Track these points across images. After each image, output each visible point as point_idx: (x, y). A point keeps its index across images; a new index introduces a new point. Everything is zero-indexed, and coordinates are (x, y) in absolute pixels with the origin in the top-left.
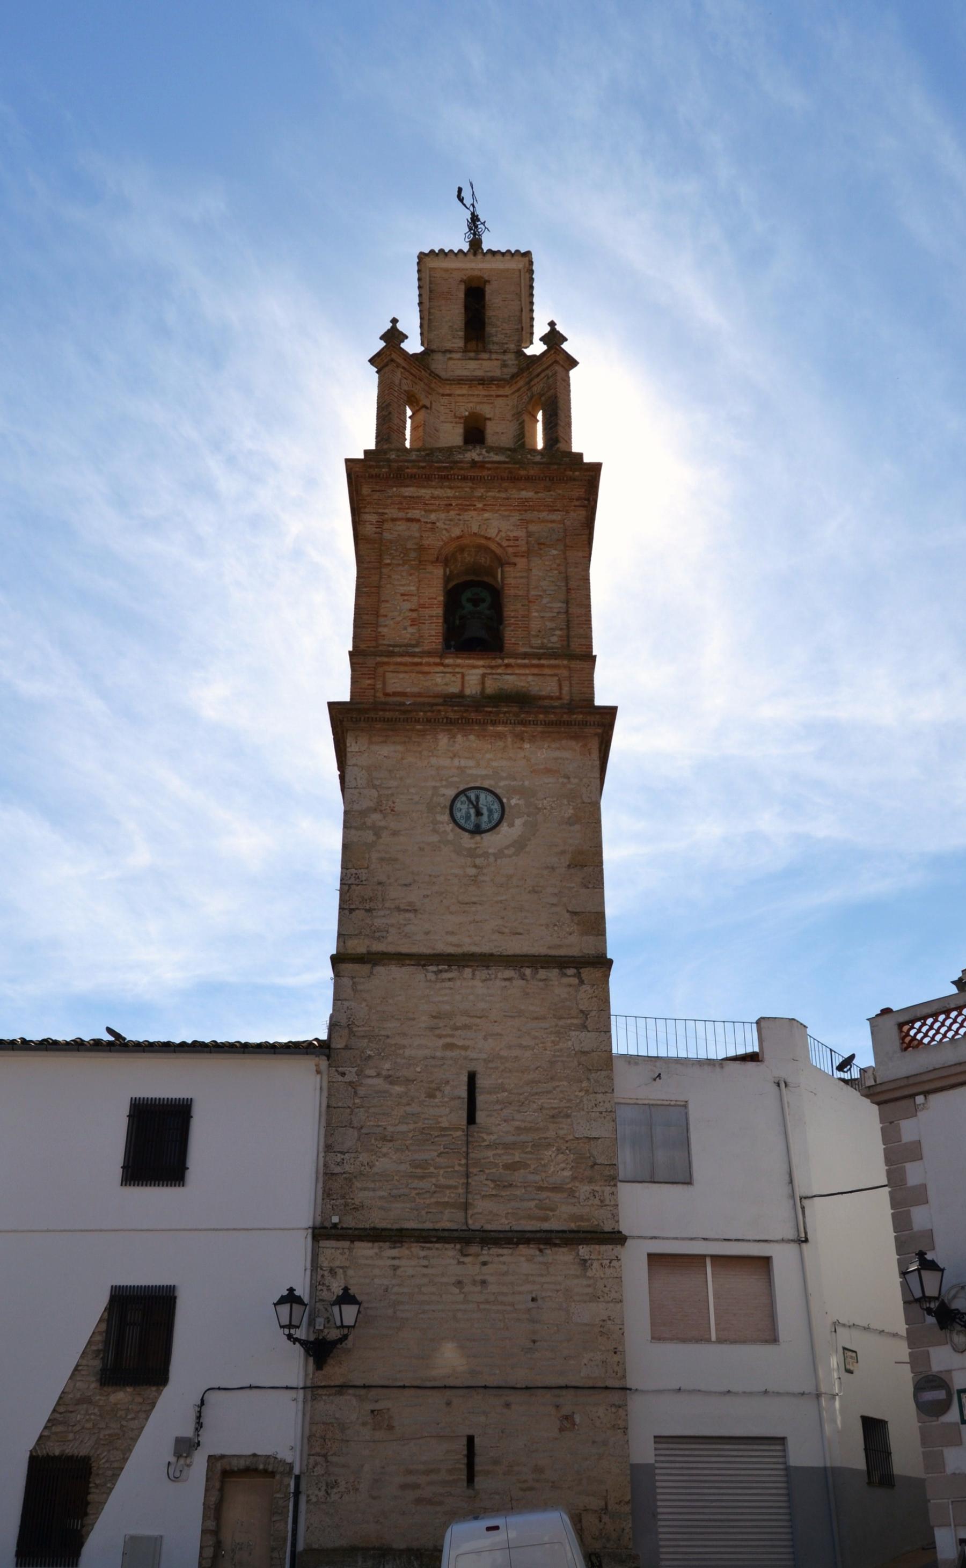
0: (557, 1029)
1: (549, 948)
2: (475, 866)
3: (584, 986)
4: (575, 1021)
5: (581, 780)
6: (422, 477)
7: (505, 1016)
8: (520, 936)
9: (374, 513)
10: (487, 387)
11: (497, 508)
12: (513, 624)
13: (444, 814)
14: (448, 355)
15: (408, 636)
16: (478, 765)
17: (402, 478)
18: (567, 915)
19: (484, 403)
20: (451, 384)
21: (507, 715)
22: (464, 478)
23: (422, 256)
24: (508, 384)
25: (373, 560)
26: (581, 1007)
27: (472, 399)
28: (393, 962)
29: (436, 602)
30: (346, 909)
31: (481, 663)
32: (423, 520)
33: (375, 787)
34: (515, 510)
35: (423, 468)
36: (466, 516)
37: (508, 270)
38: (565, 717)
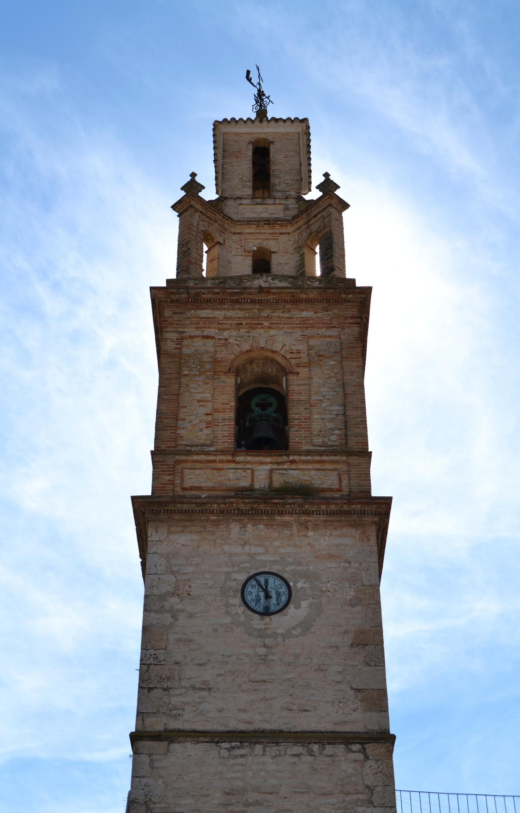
0: (345, 804)
1: (335, 724)
2: (265, 646)
3: (369, 762)
4: (361, 797)
5: (361, 564)
7: (295, 792)
8: (308, 713)
9: (174, 332)
10: (272, 227)
11: (281, 326)
12: (296, 425)
14: (239, 201)
16: (267, 552)
18: (352, 692)
19: (270, 239)
20: (241, 225)
21: (293, 506)
22: (253, 302)
24: (290, 223)
28: (188, 739)
29: (228, 407)
31: (269, 459)
32: (216, 337)
33: (172, 573)
35: (218, 293)
36: (255, 333)
37: (288, 133)
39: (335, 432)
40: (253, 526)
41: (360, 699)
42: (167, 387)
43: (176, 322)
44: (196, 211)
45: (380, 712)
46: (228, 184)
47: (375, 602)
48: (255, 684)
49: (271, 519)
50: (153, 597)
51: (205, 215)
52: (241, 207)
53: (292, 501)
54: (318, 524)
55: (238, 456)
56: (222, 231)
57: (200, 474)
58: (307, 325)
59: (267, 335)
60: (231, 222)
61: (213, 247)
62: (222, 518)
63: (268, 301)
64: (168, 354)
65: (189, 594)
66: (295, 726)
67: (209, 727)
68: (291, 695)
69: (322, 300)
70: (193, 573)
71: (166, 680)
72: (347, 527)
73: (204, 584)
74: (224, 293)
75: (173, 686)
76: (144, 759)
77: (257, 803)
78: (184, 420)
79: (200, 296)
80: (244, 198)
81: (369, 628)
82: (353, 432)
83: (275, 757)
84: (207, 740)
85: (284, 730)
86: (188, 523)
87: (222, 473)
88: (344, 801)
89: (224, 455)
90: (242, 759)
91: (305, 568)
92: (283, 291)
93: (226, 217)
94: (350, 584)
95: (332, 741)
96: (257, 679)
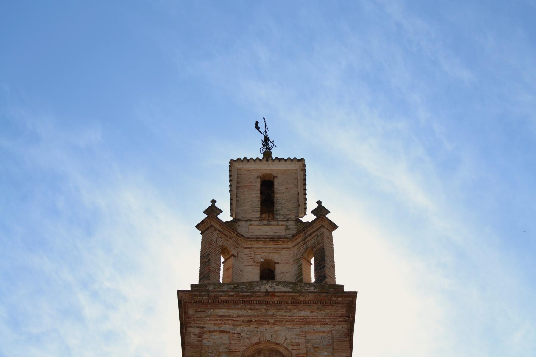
9: (197, 327)
10: (276, 243)
11: (284, 323)
14: (249, 223)
19: (274, 253)
20: (251, 241)
22: (261, 303)
23: (232, 162)
24: (290, 240)
32: (231, 331)
35: (232, 296)
36: (262, 328)
37: (288, 170)
44: (215, 230)
58: (305, 323)
61: (228, 258)
63: (273, 303)
64: (191, 346)
69: (317, 302)
74: (237, 295)
79: (218, 298)
92: (285, 294)
93: (239, 235)
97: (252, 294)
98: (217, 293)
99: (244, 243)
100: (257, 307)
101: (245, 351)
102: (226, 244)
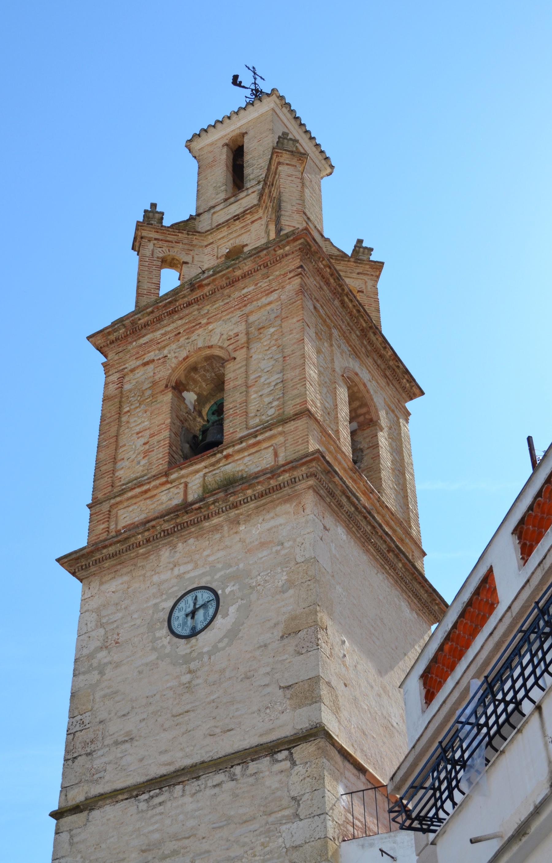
0: (268, 826)
1: (261, 735)
2: (190, 672)
3: (296, 768)
4: (286, 812)
5: (295, 541)
6: (154, 322)
7: (213, 828)
8: (232, 733)
9: (116, 372)
10: (243, 220)
11: (219, 316)
12: (231, 415)
13: (163, 628)
14: (212, 211)
15: (141, 468)
16: (196, 567)
17: (138, 331)
18: (280, 692)
19: (242, 234)
20: (211, 233)
21: (217, 504)
22: (189, 304)
23: (189, 144)
24: (259, 207)
25: (113, 414)
26: (293, 794)
27: (231, 236)
28: (108, 802)
29: (164, 426)
30: (69, 759)
31: (203, 464)
32: (156, 358)
33: (102, 625)
34: (235, 310)
35: (152, 312)
36: (194, 337)
37: (262, 115)
38: (273, 483)
39: (273, 405)
40: (183, 543)
41: (289, 697)
42: (106, 432)
43: (117, 361)
44: (149, 241)
45: (310, 705)
46: (202, 199)
47: (309, 579)
48: (178, 717)
49: (200, 529)
50: (82, 659)
51: (162, 240)
52: (215, 216)
53: (212, 499)
54: (250, 514)
55: (172, 475)
56: (188, 250)
57: (133, 510)
58: (246, 302)
59: (206, 331)
60: (199, 236)
61: (181, 270)
62: (150, 547)
63: (204, 296)
64: (108, 399)
65: (117, 643)
66: (217, 752)
67: (130, 781)
68: (215, 718)
69: (259, 268)
70: (122, 618)
71: (90, 744)
72: (282, 504)
73: (132, 626)
74: (157, 308)
75: (96, 748)
76: (65, 836)
77: (175, 853)
78: (123, 459)
79: (136, 324)
80: (217, 205)
81: (302, 610)
82: (290, 396)
83: (195, 794)
84: (126, 797)
85: (206, 760)
86: (119, 567)
87: (155, 499)
88: (267, 823)
89: (158, 478)
90: (162, 807)
91: (234, 569)
92: (215, 277)
93: (191, 233)
94: (282, 569)
95: (256, 757)
96: (180, 711)
97: (174, 298)
98: (133, 318)
99: (203, 240)
100: (186, 311)
101: (170, 375)
102: (171, 253)
